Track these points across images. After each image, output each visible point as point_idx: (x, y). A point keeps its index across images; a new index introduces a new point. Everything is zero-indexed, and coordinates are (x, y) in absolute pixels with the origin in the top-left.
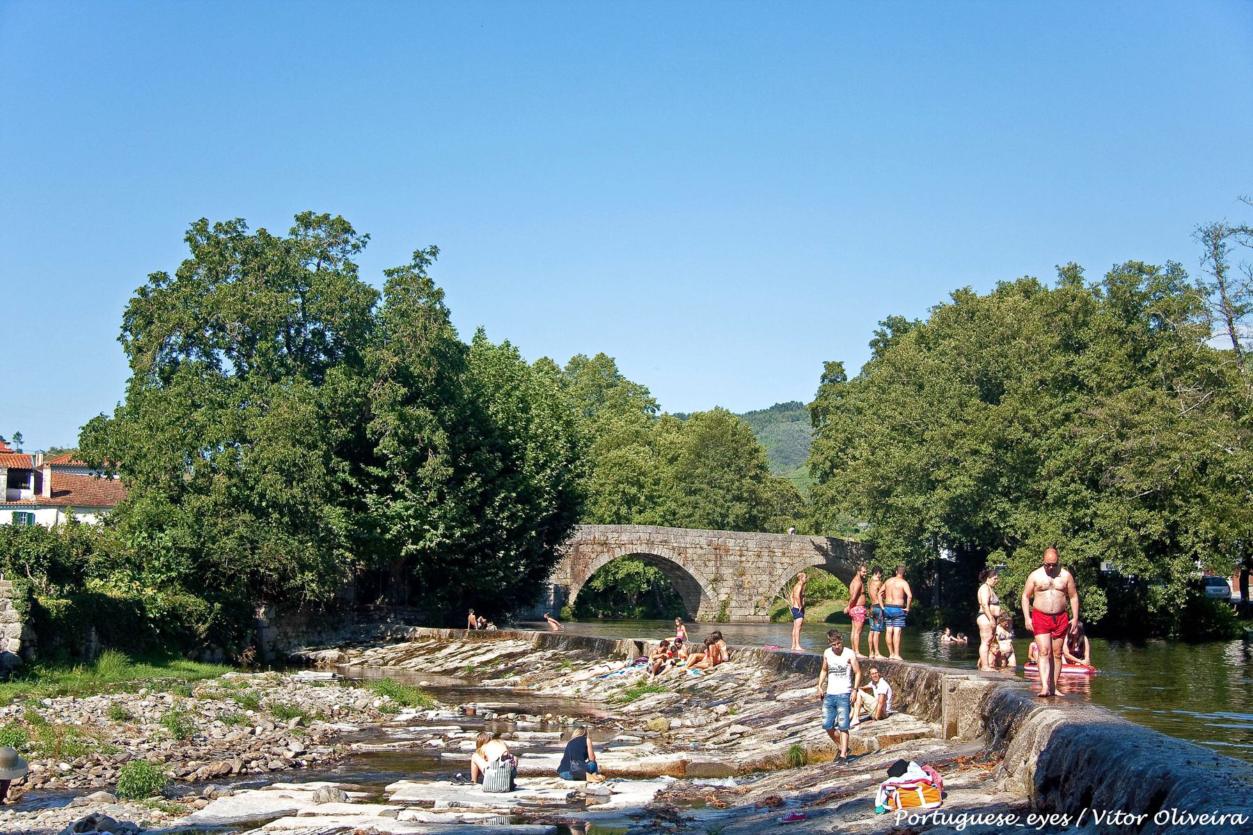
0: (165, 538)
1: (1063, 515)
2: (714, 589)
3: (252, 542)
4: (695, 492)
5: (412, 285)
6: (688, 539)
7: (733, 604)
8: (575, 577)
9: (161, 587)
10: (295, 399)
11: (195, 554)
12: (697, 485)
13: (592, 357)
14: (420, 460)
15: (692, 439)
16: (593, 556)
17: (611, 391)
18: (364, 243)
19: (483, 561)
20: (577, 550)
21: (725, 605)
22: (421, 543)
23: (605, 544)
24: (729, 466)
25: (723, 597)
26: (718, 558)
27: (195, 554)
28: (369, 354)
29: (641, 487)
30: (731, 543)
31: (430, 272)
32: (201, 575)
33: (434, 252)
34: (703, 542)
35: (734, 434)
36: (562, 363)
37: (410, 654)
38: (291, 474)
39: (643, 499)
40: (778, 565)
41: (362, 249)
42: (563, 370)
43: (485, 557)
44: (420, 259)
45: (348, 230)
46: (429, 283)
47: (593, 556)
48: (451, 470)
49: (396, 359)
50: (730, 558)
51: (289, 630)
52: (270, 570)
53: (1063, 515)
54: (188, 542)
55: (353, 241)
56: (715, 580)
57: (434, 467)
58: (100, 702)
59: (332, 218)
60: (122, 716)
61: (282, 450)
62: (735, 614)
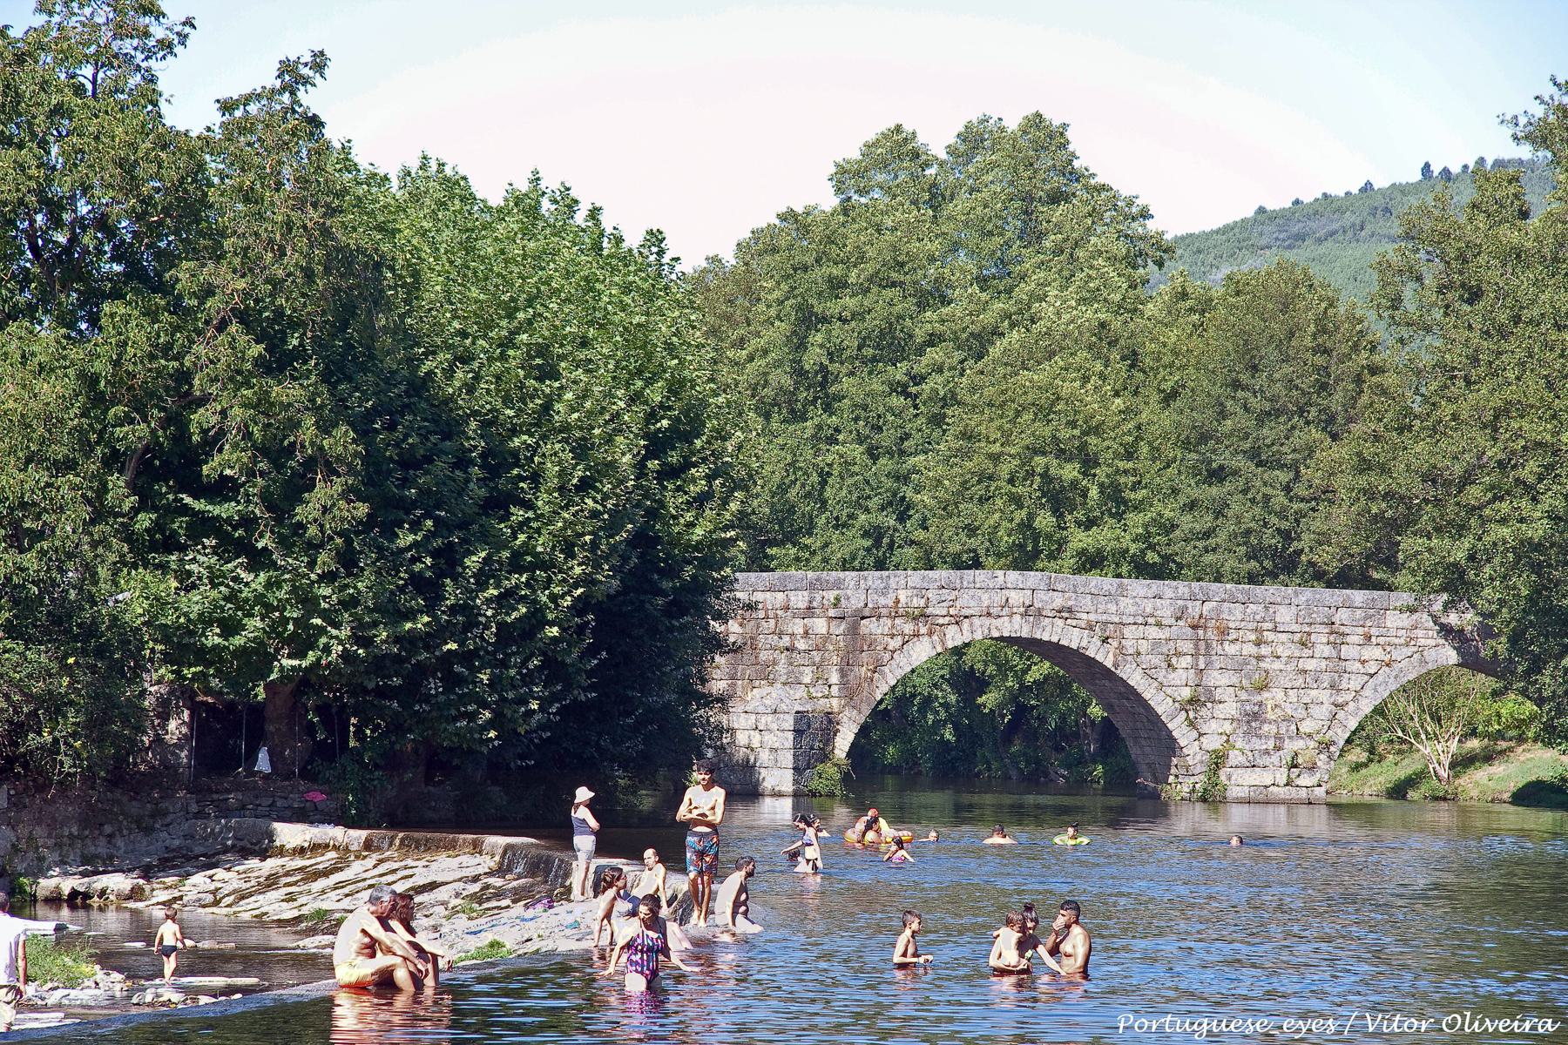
2: (1192, 724)
4: (1217, 475)
5: (280, 123)
7: (1235, 757)
8: (850, 694)
13: (1012, 124)
14: (298, 487)
19: (448, 690)
20: (854, 631)
21: (1218, 761)
22: (312, 656)
23: (922, 616)
24: (1301, 411)
25: (1213, 743)
26: (1202, 649)
29: (1089, 463)
30: (1234, 615)
34: (1166, 611)
36: (937, 139)
37: (271, 882)
39: (1094, 492)
43: (452, 681)
46: (315, 122)
47: (894, 643)
48: (362, 509)
56: (1193, 701)
57: (327, 504)
62: (1239, 782)
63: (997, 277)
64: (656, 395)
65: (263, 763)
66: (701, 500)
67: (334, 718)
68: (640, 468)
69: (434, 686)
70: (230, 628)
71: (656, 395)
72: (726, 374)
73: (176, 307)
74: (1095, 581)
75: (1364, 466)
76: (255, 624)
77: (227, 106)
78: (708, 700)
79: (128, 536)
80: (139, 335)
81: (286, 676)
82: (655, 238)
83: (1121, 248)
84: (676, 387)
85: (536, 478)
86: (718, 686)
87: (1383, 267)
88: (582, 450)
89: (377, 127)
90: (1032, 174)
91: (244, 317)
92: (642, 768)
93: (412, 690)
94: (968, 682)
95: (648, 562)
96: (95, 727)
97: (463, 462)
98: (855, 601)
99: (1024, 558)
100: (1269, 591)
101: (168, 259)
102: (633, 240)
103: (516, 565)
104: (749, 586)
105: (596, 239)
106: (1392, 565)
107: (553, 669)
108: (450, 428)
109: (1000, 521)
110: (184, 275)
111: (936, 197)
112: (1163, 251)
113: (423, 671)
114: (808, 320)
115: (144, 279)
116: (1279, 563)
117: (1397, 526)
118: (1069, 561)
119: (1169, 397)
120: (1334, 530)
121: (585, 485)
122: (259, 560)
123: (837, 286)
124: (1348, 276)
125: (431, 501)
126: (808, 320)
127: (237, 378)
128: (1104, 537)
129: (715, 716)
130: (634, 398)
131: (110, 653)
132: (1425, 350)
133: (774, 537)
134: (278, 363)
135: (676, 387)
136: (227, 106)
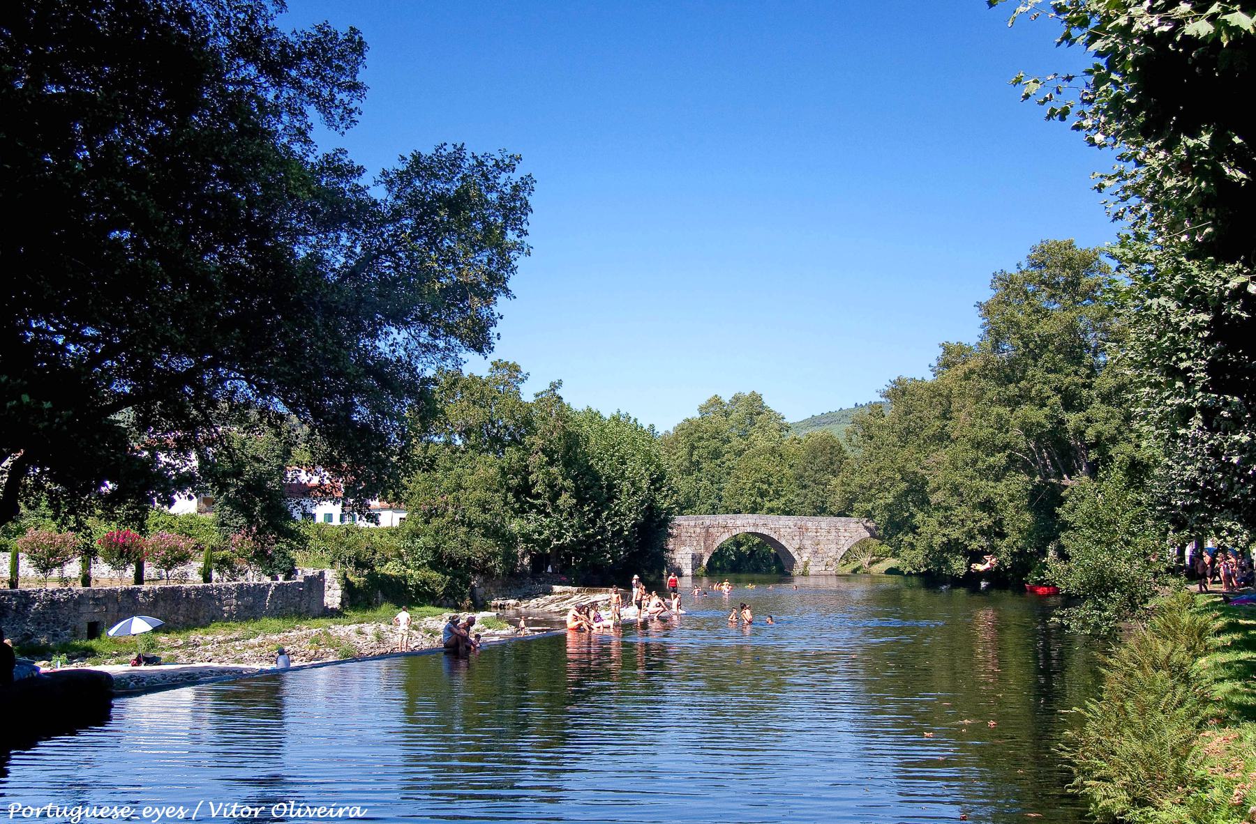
0: (419, 542)
1: (939, 515)
4: (805, 487)
5: (552, 397)
8: (707, 548)
9: (419, 568)
10: (487, 466)
11: (435, 551)
13: (747, 394)
14: (557, 496)
21: (806, 564)
25: (805, 559)
26: (802, 534)
27: (435, 551)
29: (770, 484)
30: (809, 524)
32: (439, 561)
33: (560, 383)
34: (791, 524)
36: (726, 399)
37: (552, 602)
38: (484, 507)
43: (600, 547)
46: (560, 398)
53: (939, 515)
54: (432, 544)
57: (565, 500)
58: (354, 627)
60: (360, 633)
62: (813, 570)
63: (744, 435)
64: (652, 468)
65: (550, 570)
66: (666, 496)
67: (568, 557)
68: (649, 489)
69: (595, 548)
70: (540, 533)
71: (652, 468)
72: (671, 463)
73: (525, 449)
74: (772, 516)
75: (843, 484)
76: (547, 532)
77: (537, 396)
78: (668, 551)
79: (513, 509)
80: (515, 457)
81: (556, 546)
82: (652, 426)
83: (777, 427)
84: (658, 466)
85: (621, 491)
86: (671, 547)
87: (847, 431)
88: (633, 484)
89: (576, 399)
90: (754, 408)
91: (543, 451)
92: (651, 571)
93: (589, 549)
94: (738, 544)
95: (652, 514)
96: (505, 561)
97: (601, 487)
98: (708, 523)
99: (754, 510)
100: (819, 518)
101: (522, 435)
102: (646, 427)
103: (616, 514)
104: (679, 520)
105: (637, 428)
106: (852, 511)
107: (626, 543)
108: (598, 479)
109: (746, 501)
110: (527, 440)
111: (727, 414)
112: (788, 428)
113: (592, 544)
114: (693, 448)
115: (516, 442)
116: (821, 510)
117: (854, 500)
118: (765, 510)
119: (791, 466)
120: (836, 501)
121: (634, 493)
122: (547, 515)
123: (701, 438)
124: (839, 432)
125: (592, 498)
126: (693, 448)
127: (541, 467)
128: (774, 504)
129: (670, 555)
130: (647, 470)
131: (508, 540)
132: (859, 453)
133: (687, 506)
134: (551, 463)
135: (658, 466)
136: (537, 396)
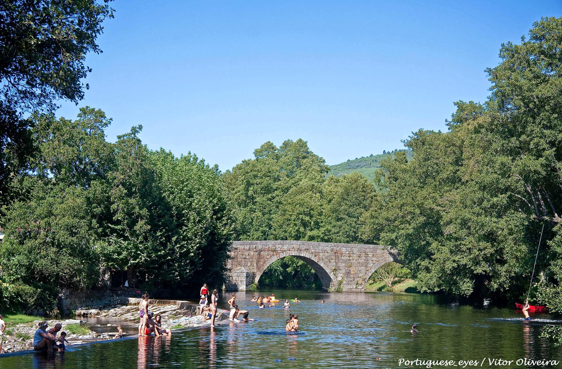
3: (56, 261)
6: (320, 248)
7: (344, 282)
8: (258, 268)
10: (75, 197)
12: (342, 216)
13: (295, 141)
15: (340, 190)
16: (268, 257)
17: (305, 161)
18: (110, 123)
19: (168, 268)
21: (340, 283)
22: (138, 260)
25: (340, 279)
26: (337, 258)
28: (109, 175)
30: (344, 250)
31: (139, 136)
33: (141, 127)
34: (329, 249)
35: (364, 187)
36: (278, 144)
37: (128, 311)
40: (370, 262)
41: (109, 125)
42: (279, 148)
43: (169, 266)
44: (135, 131)
45: (103, 116)
47: (268, 257)
48: (149, 227)
49: (122, 177)
50: (343, 258)
51: (76, 300)
52: (65, 274)
53: (452, 243)
55: (104, 121)
57: (141, 226)
59: (96, 110)
61: (68, 220)
